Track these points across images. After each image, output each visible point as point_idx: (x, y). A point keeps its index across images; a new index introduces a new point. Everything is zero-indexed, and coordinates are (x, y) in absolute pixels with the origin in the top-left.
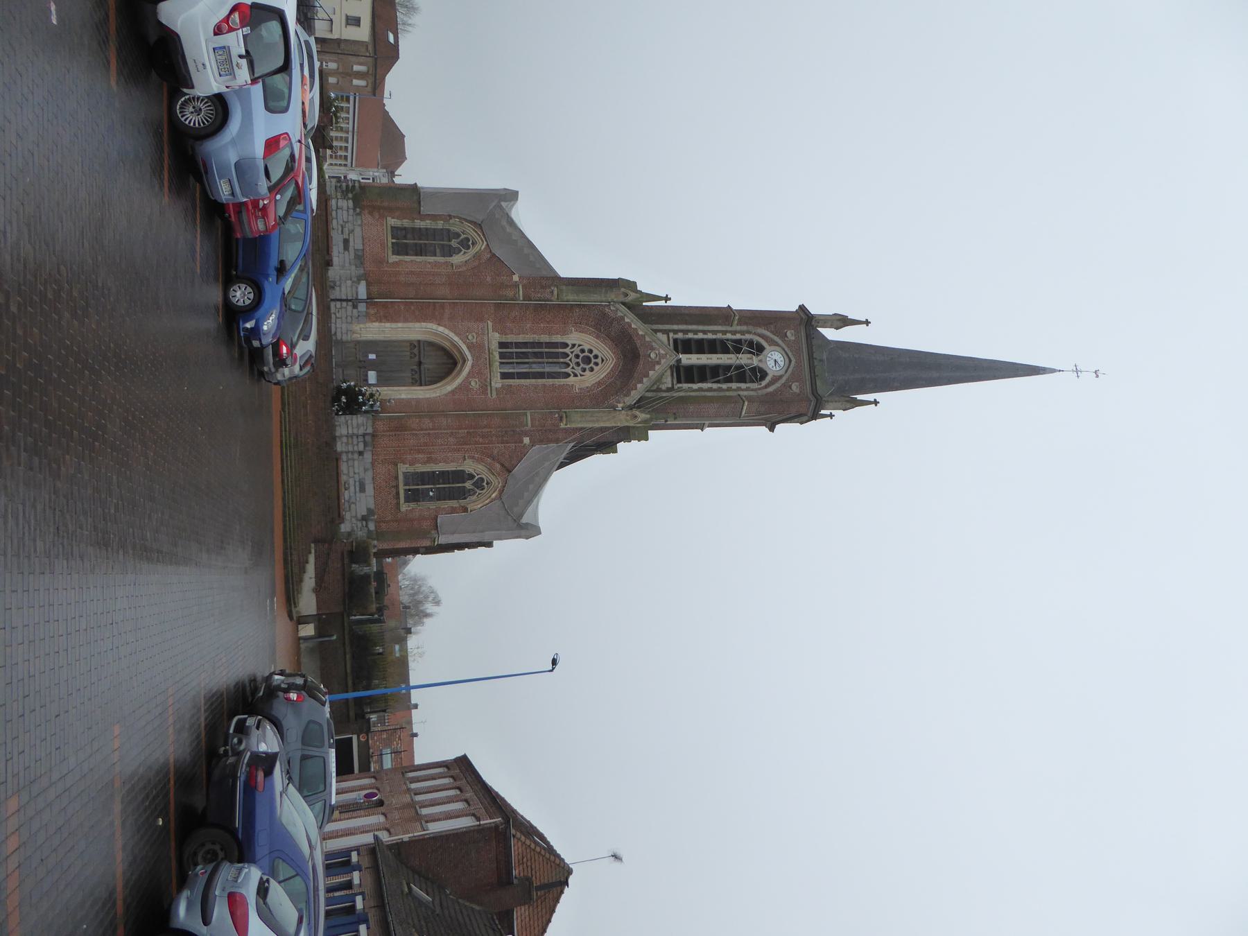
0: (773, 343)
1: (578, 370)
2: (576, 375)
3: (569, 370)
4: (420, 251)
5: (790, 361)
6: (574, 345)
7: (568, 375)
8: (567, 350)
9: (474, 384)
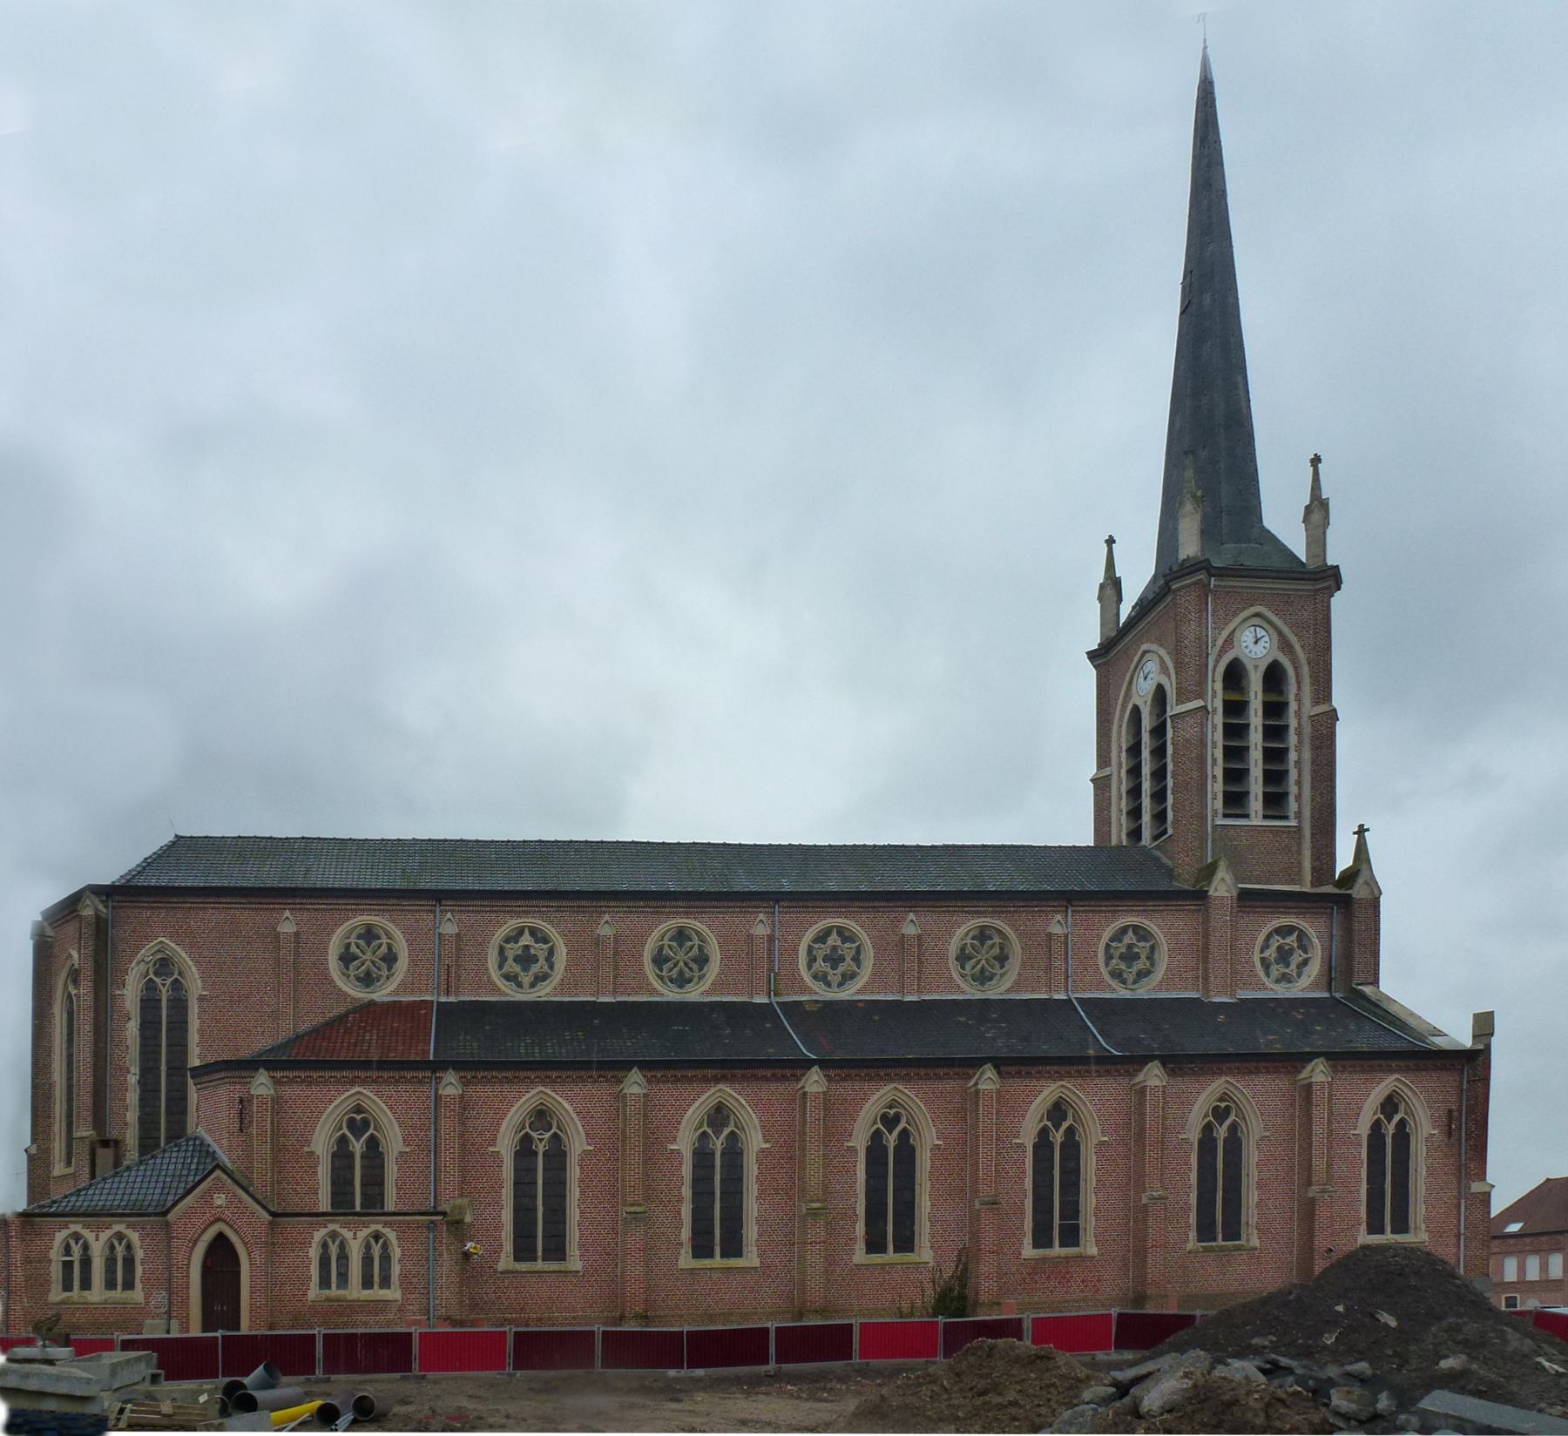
0: (1229, 641)
4: (1071, 1209)
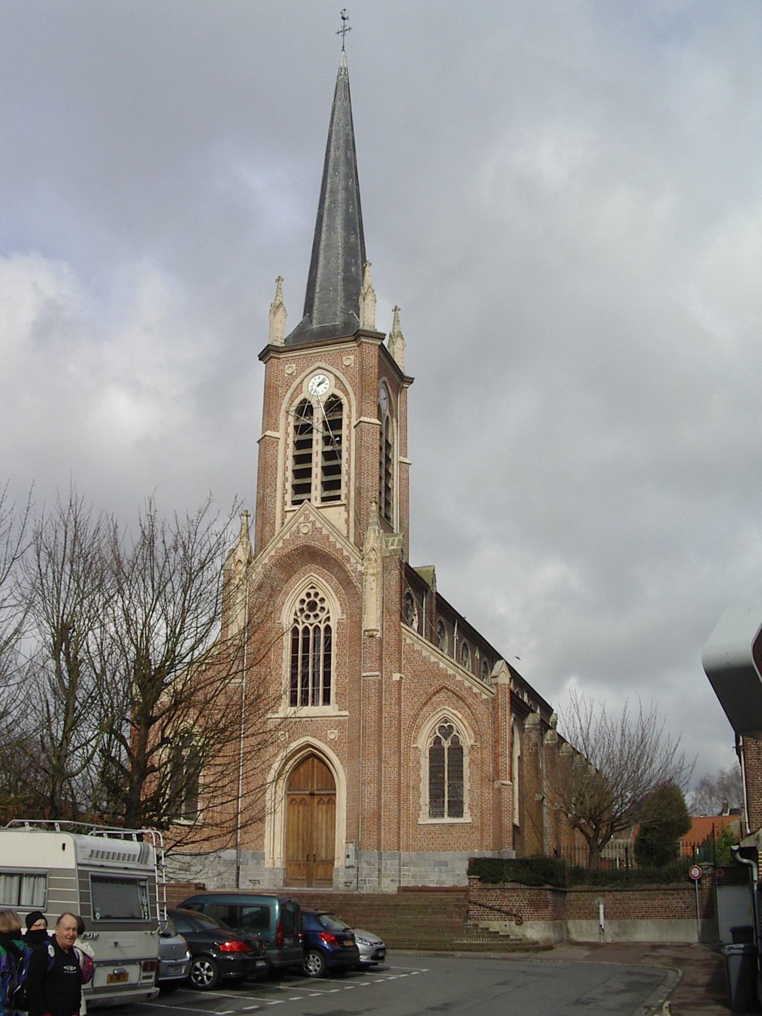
1: (323, 616)
2: (328, 619)
3: (322, 627)
5: (319, 368)
6: (296, 621)
7: (328, 629)
8: (300, 628)
9: (333, 735)
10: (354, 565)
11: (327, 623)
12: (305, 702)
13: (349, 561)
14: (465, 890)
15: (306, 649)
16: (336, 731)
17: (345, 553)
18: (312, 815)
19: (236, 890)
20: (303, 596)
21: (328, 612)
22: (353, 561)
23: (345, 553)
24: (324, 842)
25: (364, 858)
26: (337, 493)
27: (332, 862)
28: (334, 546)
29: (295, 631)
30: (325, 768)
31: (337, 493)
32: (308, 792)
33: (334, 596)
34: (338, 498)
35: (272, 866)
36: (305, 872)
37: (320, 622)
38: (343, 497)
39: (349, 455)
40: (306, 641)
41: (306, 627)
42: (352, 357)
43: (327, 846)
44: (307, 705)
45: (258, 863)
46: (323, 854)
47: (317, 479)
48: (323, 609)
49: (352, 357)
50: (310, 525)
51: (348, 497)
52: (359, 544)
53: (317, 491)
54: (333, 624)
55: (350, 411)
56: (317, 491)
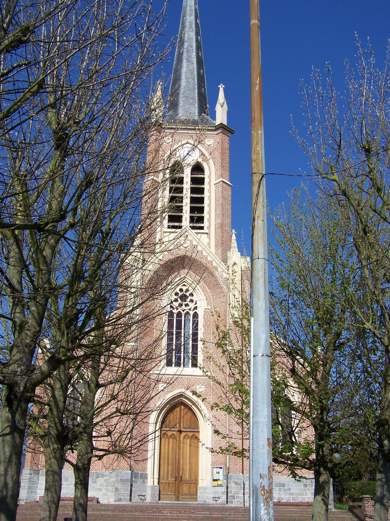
3: (192, 313)
7: (196, 315)
8: (175, 311)
10: (221, 272)
11: (195, 310)
12: (178, 364)
13: (217, 270)
14: (309, 505)
15: (179, 327)
16: (203, 387)
17: (214, 264)
18: (179, 446)
19: (130, 503)
20: (178, 290)
21: (196, 304)
22: (220, 270)
23: (214, 264)
24: (188, 466)
25: (233, 480)
26: (201, 225)
27: (196, 482)
28: (206, 258)
29: (171, 314)
30: (190, 413)
31: (201, 225)
32: (177, 430)
33: (202, 293)
34: (202, 228)
35: (152, 484)
36: (173, 489)
37: (190, 309)
38: (205, 228)
39: (210, 201)
40: (179, 323)
41: (179, 312)
42: (212, 141)
43: (190, 470)
44: (171, 366)
45: (144, 482)
46: (187, 476)
47: (186, 215)
48: (192, 301)
49: (212, 141)
50: (189, 242)
51: (209, 228)
52: (225, 260)
53: (186, 222)
54: (200, 312)
55: (210, 174)
56: (186, 222)
